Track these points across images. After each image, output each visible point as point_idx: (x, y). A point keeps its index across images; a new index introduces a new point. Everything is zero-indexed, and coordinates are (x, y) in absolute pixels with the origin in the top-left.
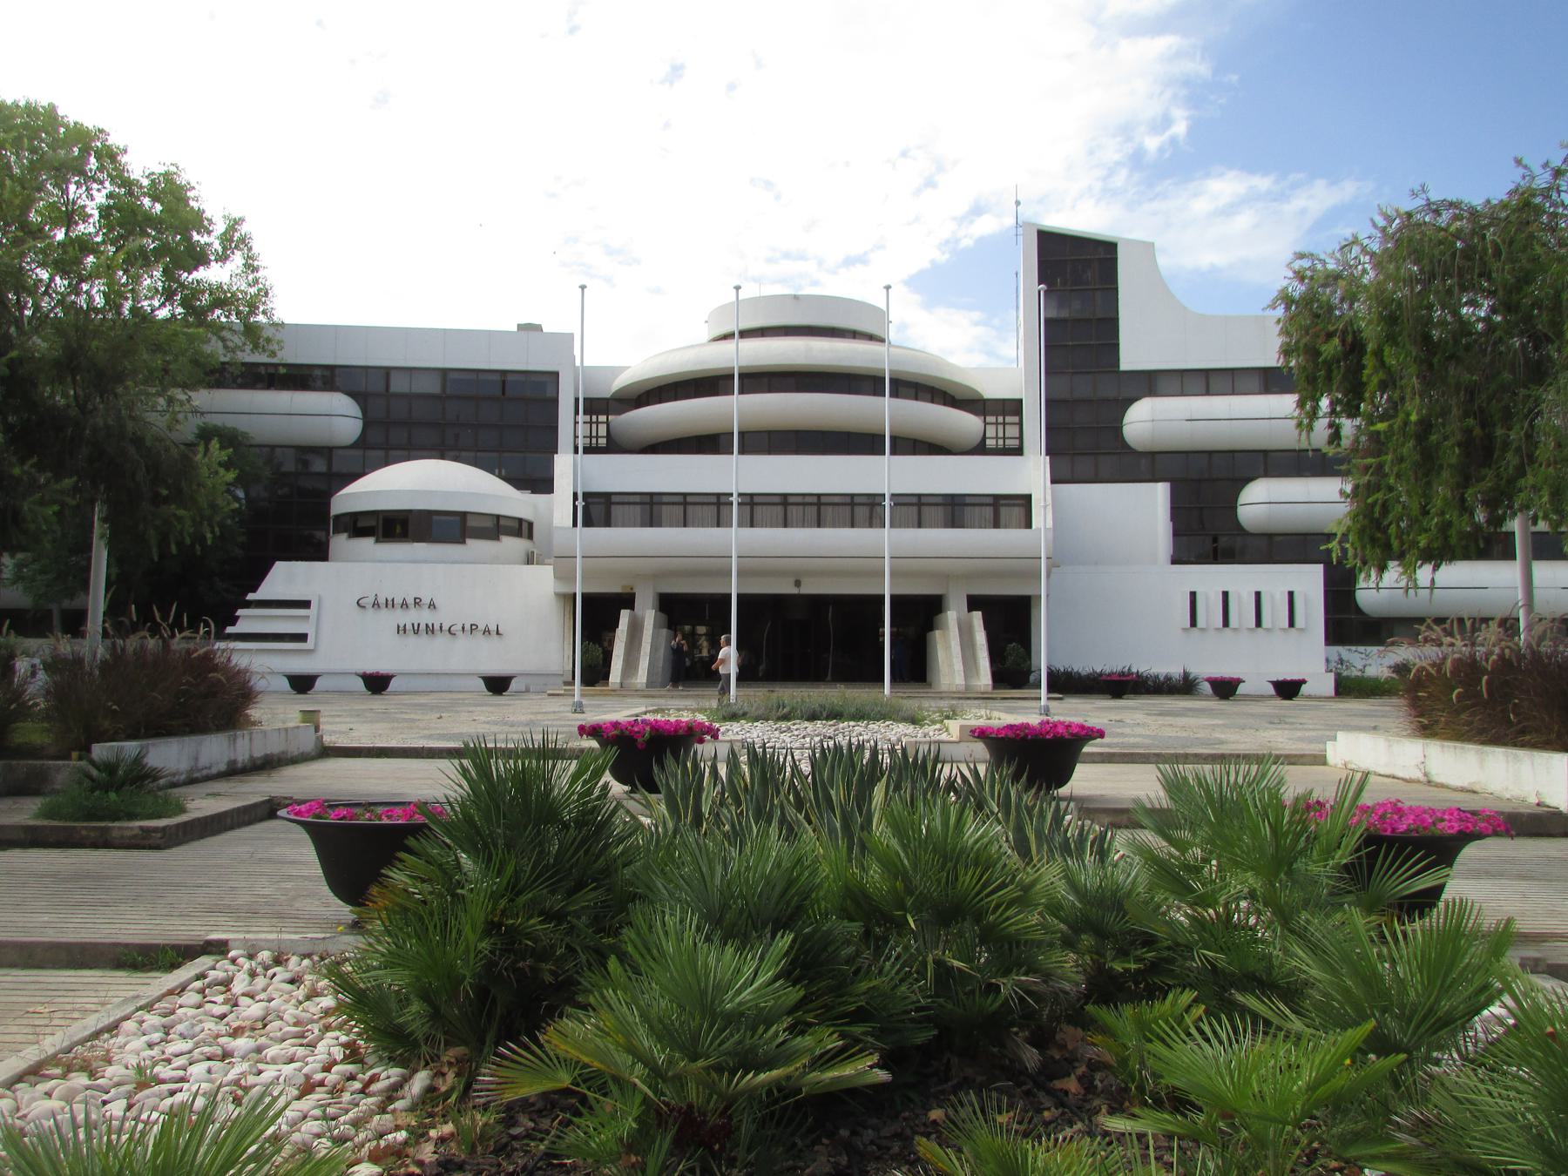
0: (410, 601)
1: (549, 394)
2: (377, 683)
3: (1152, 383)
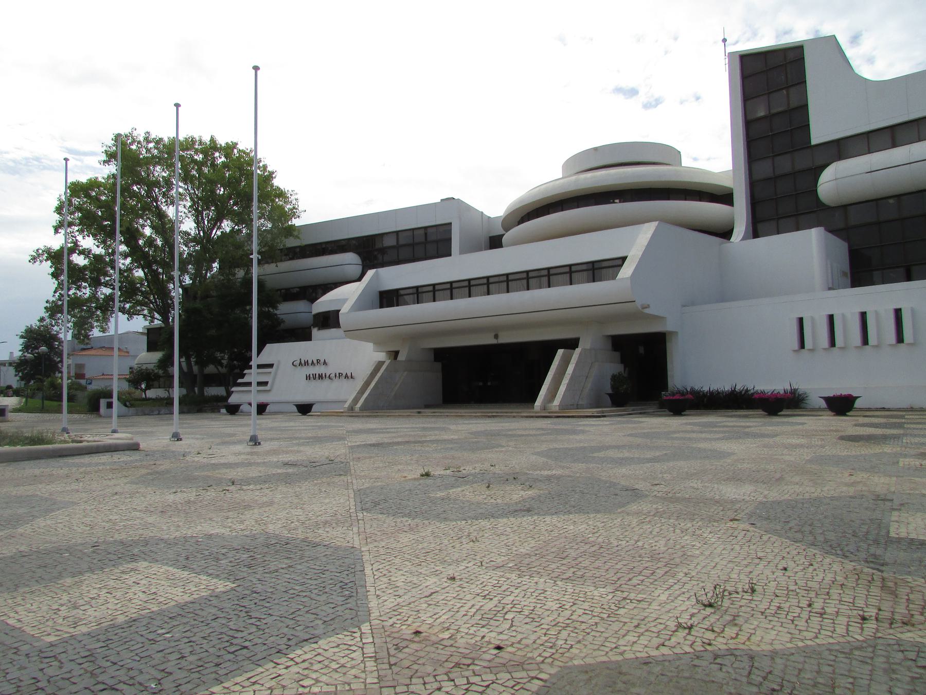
0: (315, 362)
1: (422, 232)
2: (304, 409)
3: (840, 149)
